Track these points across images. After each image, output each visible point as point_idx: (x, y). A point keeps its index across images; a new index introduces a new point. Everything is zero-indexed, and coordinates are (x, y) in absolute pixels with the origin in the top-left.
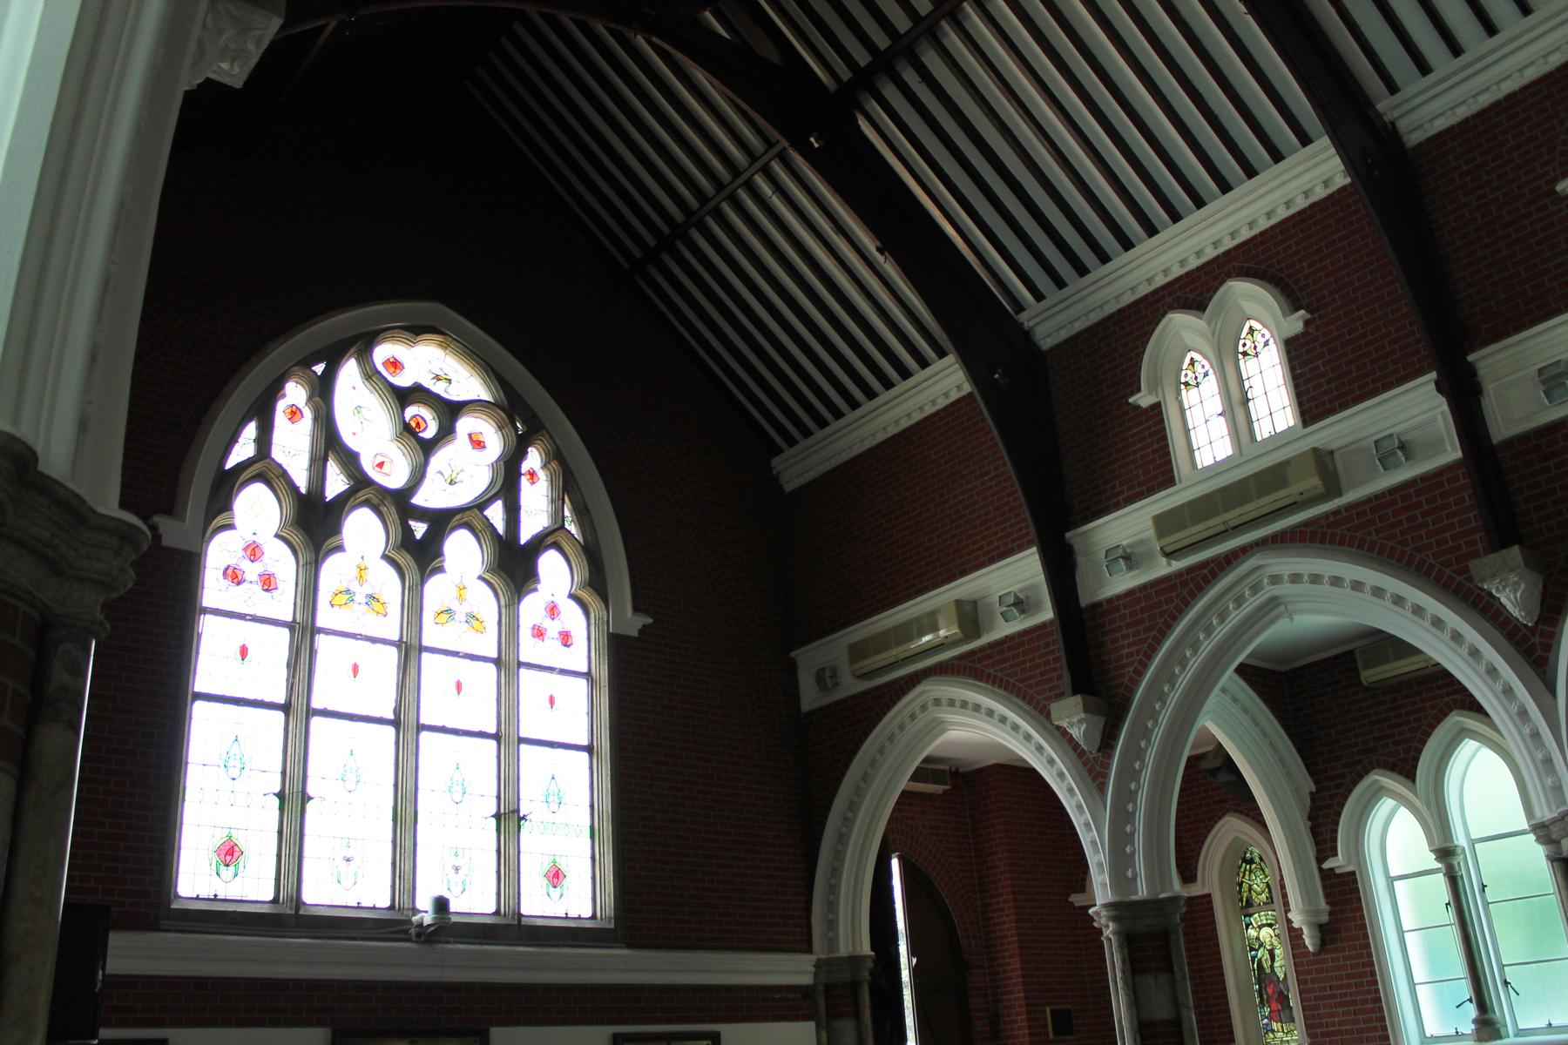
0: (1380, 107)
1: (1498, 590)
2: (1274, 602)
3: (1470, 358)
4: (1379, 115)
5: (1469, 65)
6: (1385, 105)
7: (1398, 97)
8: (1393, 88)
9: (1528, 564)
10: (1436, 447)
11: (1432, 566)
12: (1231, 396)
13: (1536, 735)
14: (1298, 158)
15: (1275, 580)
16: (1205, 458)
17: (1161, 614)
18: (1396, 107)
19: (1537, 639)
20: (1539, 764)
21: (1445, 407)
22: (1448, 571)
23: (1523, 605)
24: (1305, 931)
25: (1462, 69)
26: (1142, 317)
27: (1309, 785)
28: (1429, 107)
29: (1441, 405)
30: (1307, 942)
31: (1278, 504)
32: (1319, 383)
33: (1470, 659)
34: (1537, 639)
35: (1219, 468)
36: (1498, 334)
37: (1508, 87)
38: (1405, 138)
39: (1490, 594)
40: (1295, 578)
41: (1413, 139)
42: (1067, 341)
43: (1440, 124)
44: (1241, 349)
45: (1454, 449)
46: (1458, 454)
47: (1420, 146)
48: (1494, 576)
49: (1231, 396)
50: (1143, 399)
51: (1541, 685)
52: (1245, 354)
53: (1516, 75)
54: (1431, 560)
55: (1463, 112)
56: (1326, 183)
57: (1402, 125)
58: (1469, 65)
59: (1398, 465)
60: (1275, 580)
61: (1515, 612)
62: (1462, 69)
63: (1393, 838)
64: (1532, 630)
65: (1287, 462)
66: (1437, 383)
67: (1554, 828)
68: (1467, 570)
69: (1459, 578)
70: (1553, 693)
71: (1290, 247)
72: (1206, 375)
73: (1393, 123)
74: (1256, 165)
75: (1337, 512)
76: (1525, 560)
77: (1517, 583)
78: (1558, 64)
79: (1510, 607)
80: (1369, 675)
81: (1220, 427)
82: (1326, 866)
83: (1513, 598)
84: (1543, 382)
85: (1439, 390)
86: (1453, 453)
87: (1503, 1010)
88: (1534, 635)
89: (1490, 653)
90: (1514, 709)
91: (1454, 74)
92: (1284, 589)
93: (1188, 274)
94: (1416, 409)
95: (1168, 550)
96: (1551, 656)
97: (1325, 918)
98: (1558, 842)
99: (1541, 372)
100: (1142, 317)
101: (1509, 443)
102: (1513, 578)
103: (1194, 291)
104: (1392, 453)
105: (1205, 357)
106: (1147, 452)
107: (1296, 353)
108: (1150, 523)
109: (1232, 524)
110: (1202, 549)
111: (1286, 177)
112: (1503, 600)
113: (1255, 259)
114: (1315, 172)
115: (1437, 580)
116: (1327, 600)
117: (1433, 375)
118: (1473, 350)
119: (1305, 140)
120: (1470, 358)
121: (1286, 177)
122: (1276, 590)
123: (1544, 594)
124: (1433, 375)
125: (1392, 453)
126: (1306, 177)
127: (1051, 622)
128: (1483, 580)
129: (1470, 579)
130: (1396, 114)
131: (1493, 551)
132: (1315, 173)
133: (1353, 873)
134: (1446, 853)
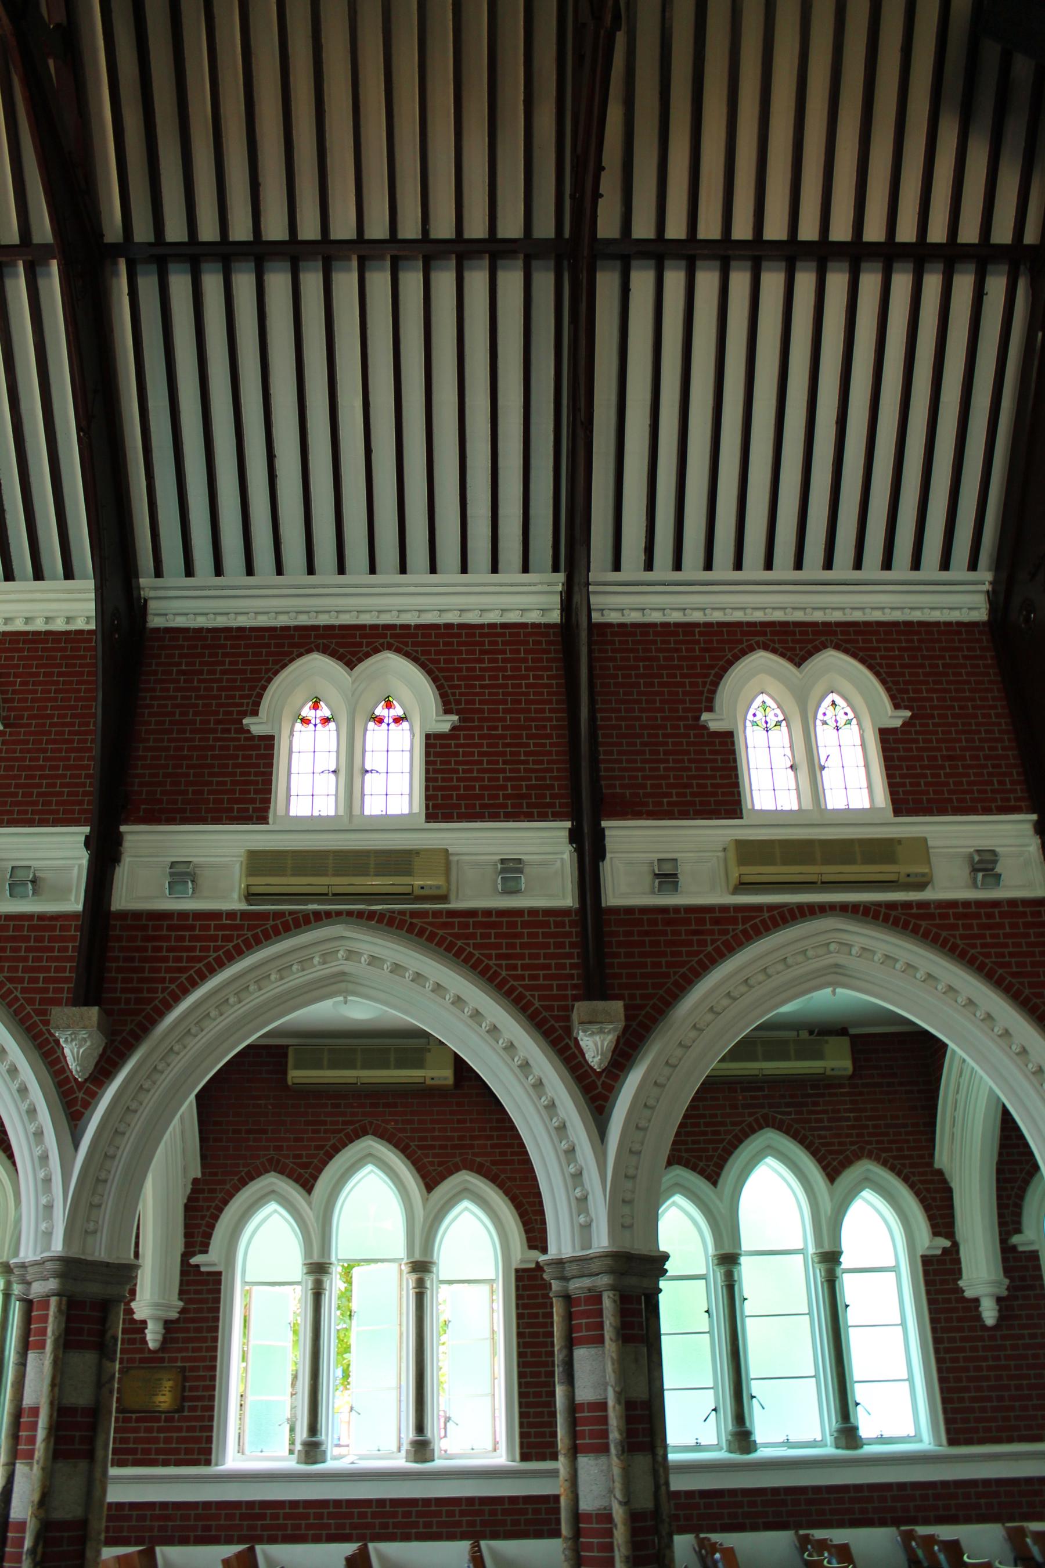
0: (142, 581)
1: (66, 1041)
2: (341, 976)
3: (123, 828)
4: (139, 588)
5: (223, 588)
6: (146, 582)
7: (159, 581)
8: (158, 573)
9: (100, 1027)
10: (62, 893)
11: (16, 999)
12: (349, 761)
13: (48, 1181)
14: (55, 586)
15: (351, 955)
16: (299, 808)
17: (217, 949)
18: (155, 589)
19: (81, 1095)
20: (41, 1208)
21: (85, 862)
22: (29, 1008)
23: (81, 1061)
24: (150, 1325)
25: (216, 588)
26: (274, 649)
27: (196, 1171)
28: (180, 603)
29: (81, 858)
30: (149, 1337)
31: (816, 874)
32: (453, 784)
33: (16, 1095)
34: (81, 1095)
35: (314, 825)
36: (152, 818)
37: (243, 621)
38: (150, 618)
39: (57, 1042)
40: (374, 960)
41: (155, 622)
42: (796, 624)
43: (180, 622)
44: (820, 716)
45: (77, 902)
46: (79, 907)
47: (157, 630)
48: (68, 1027)
49: (349, 761)
50: (256, 726)
51: (69, 1137)
52: (755, 724)
53: (395, 613)
54: (18, 994)
55: (201, 622)
56: (69, 620)
57: (152, 606)
58: (223, 588)
59: (24, 897)
60: (351, 955)
61: (72, 1064)
62: (216, 588)
63: (265, 1242)
64: (80, 1085)
65: (899, 841)
66: (87, 837)
67: (30, 1270)
68: (43, 1013)
69: (36, 1018)
70: (76, 1146)
71: (12, 658)
72: (849, 722)
73: (146, 601)
74: (46, 573)
75: (907, 905)
76: (99, 1024)
77: (85, 1040)
78: (283, 624)
79: (70, 1059)
80: (296, 1075)
81: (328, 784)
82: (194, 1261)
83: (76, 1051)
84: (172, 874)
85: (87, 844)
86: (75, 903)
87: (433, 1430)
88: (80, 1090)
89: (37, 1095)
90: (38, 1152)
91: (209, 588)
92: (357, 968)
93: (48, 633)
94: (544, 847)
95: (255, 890)
96: (87, 1113)
97: (174, 1315)
98: (29, 1284)
99: (173, 864)
100: (274, 649)
101: (124, 915)
102: (83, 1034)
103: (351, 644)
104: (23, 883)
105: (850, 705)
106: (246, 783)
107: (436, 750)
108: (242, 851)
109: (826, 878)
110: (757, 892)
111: (38, 596)
112: (67, 1051)
113: (436, 649)
114: (527, 598)
115: (16, 1013)
116: (378, 989)
117: (87, 829)
118: (126, 822)
119: (69, 574)
120: (123, 828)
121: (38, 596)
122: (349, 967)
123: (101, 1056)
124: (87, 829)
125: (23, 883)
126: (54, 606)
127: (74, 916)
128: (57, 1028)
129: (46, 1023)
130: (152, 594)
131: (75, 1005)
132: (64, 606)
133: (220, 1273)
134: (318, 1269)
